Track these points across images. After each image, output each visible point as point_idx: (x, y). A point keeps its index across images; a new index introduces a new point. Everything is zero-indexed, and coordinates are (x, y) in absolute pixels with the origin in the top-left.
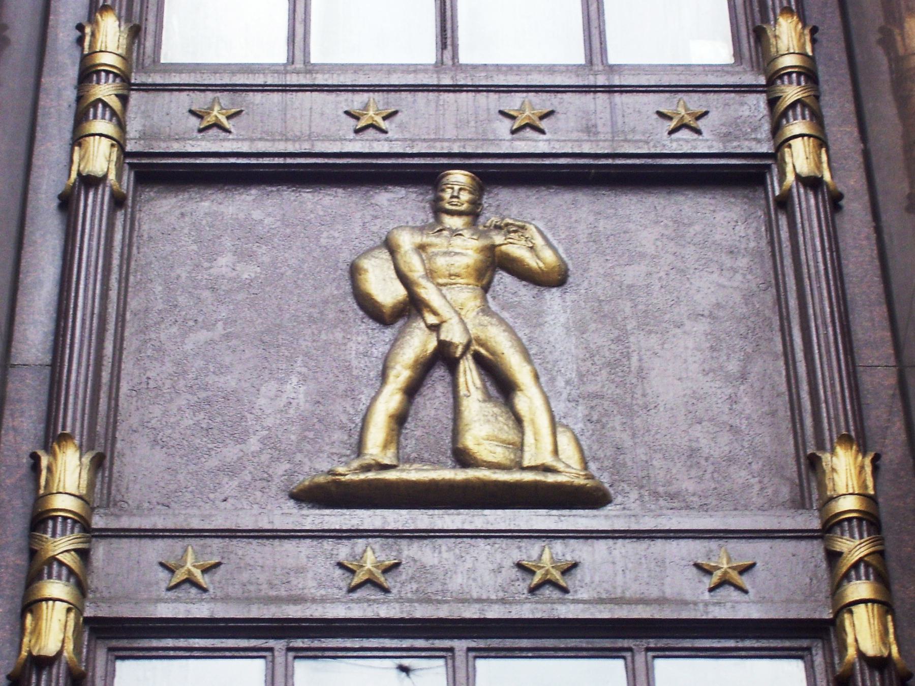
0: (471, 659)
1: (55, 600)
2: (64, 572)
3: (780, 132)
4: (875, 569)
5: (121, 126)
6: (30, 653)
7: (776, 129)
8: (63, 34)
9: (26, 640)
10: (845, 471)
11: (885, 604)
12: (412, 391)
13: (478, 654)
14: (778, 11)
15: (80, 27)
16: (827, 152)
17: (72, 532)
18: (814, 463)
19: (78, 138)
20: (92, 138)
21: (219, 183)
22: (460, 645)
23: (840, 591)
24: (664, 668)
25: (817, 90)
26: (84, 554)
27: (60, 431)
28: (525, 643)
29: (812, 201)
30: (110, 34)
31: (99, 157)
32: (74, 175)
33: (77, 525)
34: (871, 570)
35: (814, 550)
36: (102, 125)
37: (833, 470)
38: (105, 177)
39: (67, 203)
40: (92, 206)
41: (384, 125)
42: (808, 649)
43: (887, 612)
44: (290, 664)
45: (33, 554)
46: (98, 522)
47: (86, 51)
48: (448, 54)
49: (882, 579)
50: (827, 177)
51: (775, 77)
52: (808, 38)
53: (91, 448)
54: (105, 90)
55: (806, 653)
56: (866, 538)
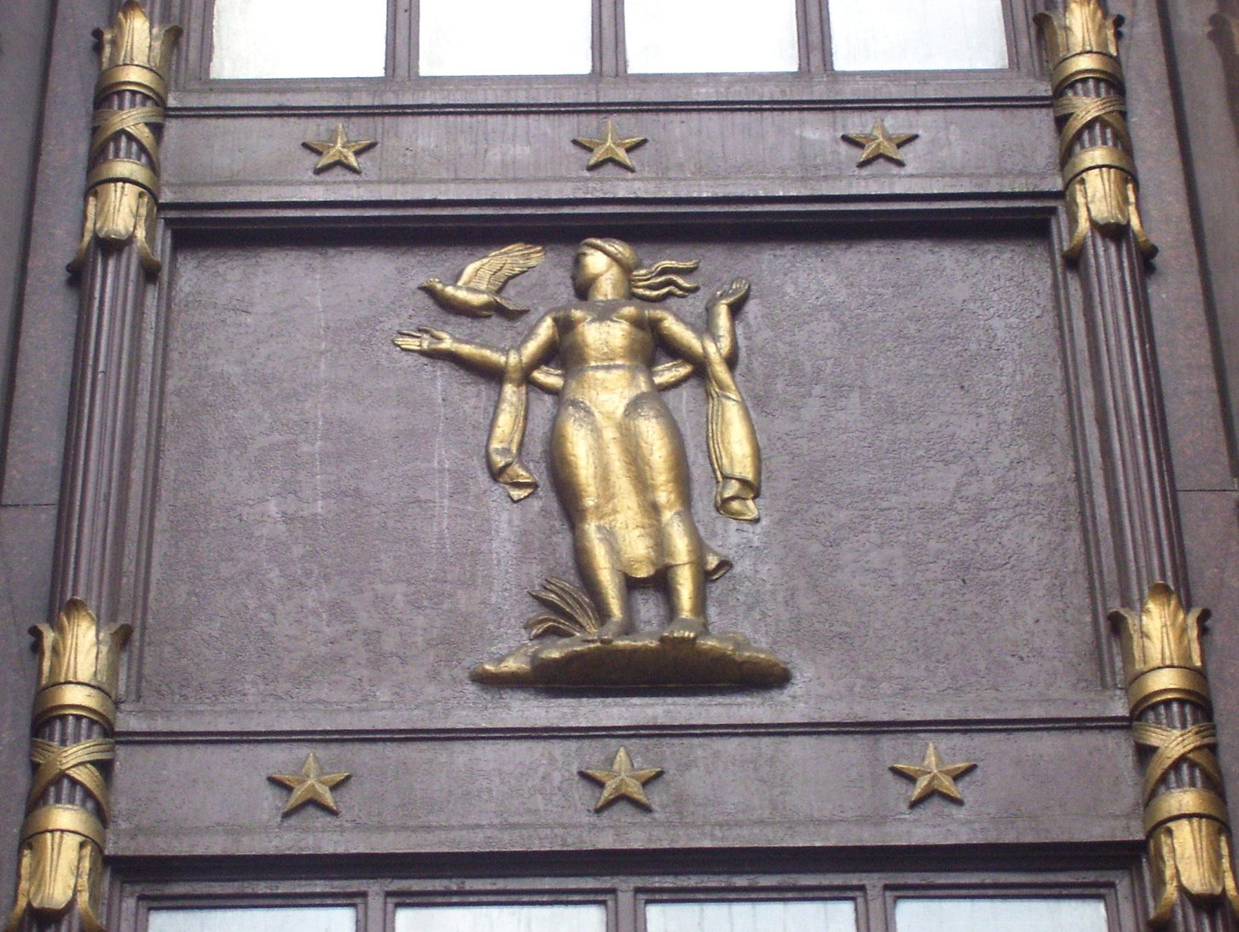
0: (142, 911)
3: (1071, 162)
4: (1203, 771)
6: (29, 904)
9: (24, 885)
11: (1218, 822)
13: (898, 893)
16: (1136, 190)
18: (1117, 625)
19: (95, 186)
21: (459, 244)
22: (374, 888)
25: (1124, 103)
26: (104, 767)
27: (69, 596)
28: (320, 886)
30: (139, 33)
31: (122, 211)
32: (88, 237)
33: (96, 729)
34: (1197, 773)
35: (1118, 747)
38: (131, 239)
40: (112, 281)
42: (364, 895)
43: (1220, 832)
45: (35, 767)
46: (129, 722)
48: (816, 58)
49: (1214, 785)
50: (1135, 222)
51: (1065, 86)
52: (1110, 33)
55: (858, 893)
56: (1190, 727)
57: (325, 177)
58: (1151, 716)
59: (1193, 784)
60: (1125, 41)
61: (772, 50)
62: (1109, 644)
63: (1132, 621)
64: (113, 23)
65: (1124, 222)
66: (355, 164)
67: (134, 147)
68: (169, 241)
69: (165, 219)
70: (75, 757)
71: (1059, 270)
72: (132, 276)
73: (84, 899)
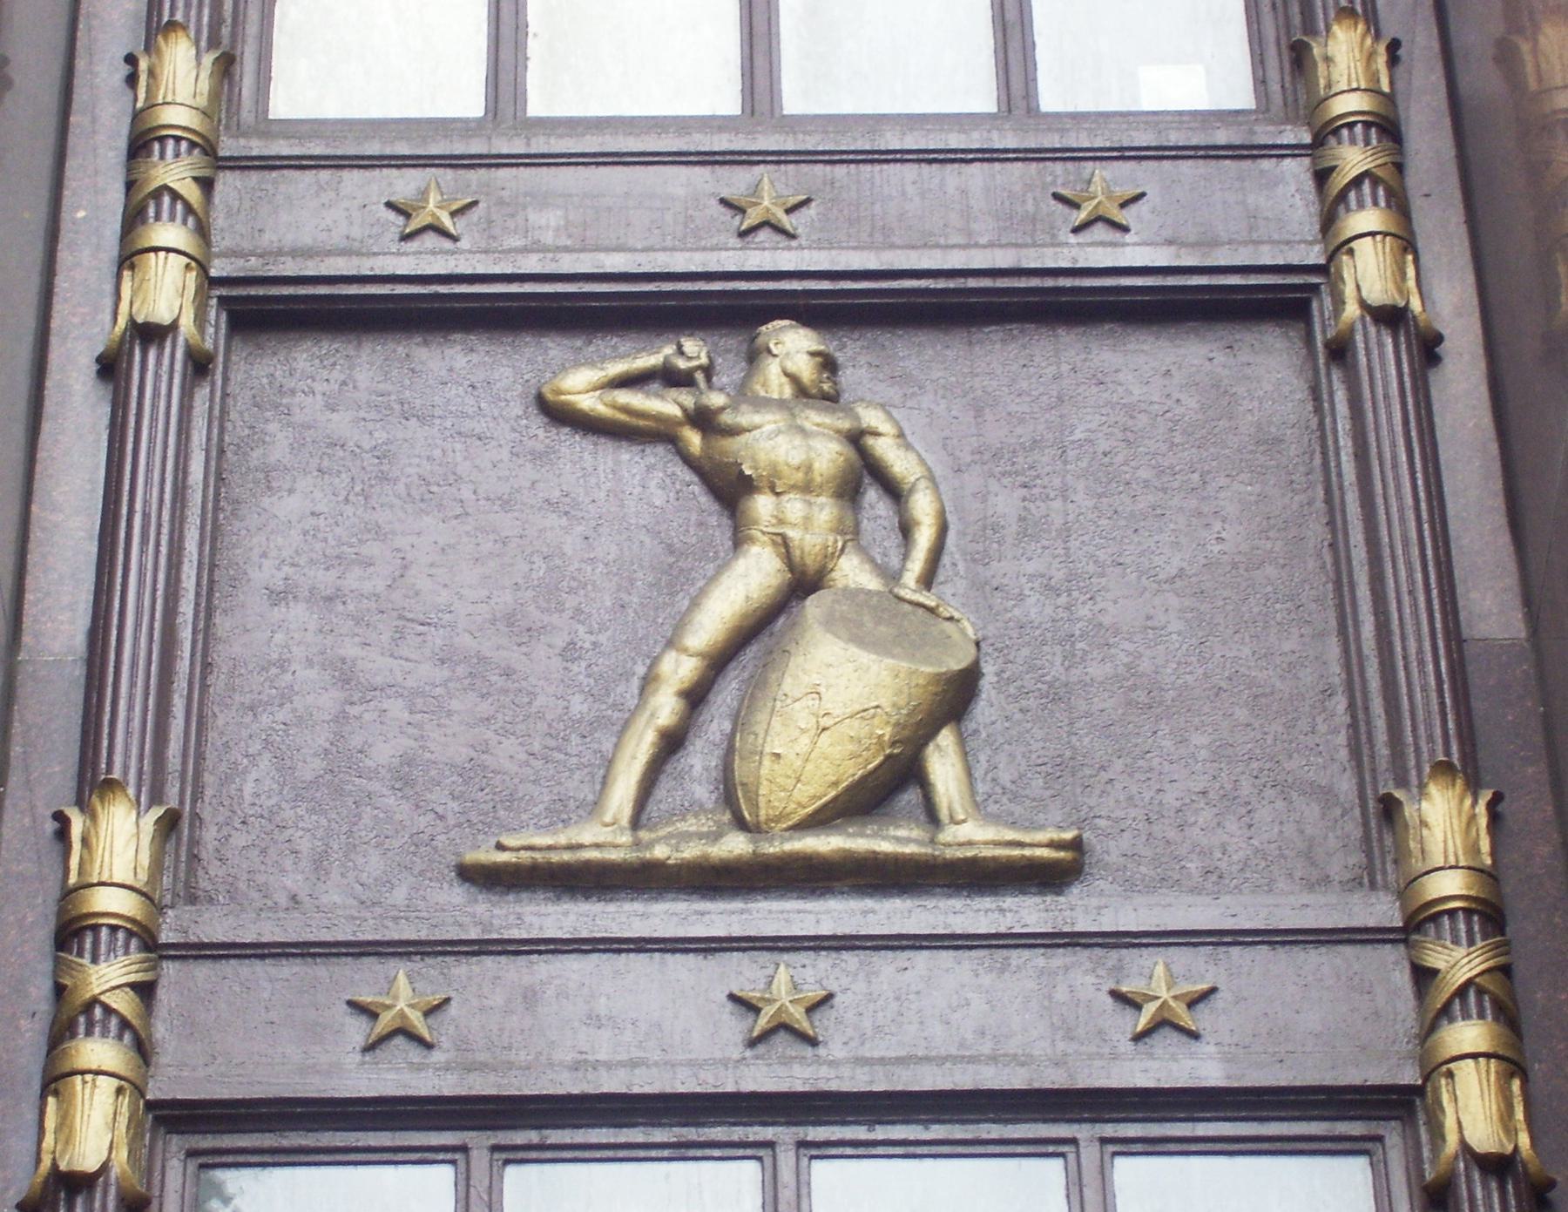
1: (98, 1073)
2: (114, 1022)
5: (202, 231)
6: (55, 1165)
7: (1328, 221)
8: (101, 76)
10: (1443, 820)
11: (1511, 1063)
12: (696, 697)
13: (1117, 1148)
14: (1332, 14)
15: (131, 60)
16: (1416, 261)
17: (127, 953)
18: (1389, 809)
19: (129, 257)
20: (152, 255)
23: (1435, 1037)
24: (1130, 1172)
26: (145, 991)
27: (166, 19)
29: (1390, 348)
30: (183, 75)
32: (122, 322)
34: (1381, 192)
35: (1390, 966)
36: (169, 233)
37: (1424, 824)
39: (110, 367)
40: (157, 374)
41: (787, 222)
43: (1405, 250)
44: (803, 1170)
47: (140, 105)
49: (1507, 1015)
50: (1416, 304)
51: (1326, 133)
53: (156, 798)
54: (174, 171)
56: (1480, 944)
57: (413, 245)
58: (1431, 927)
59: (1481, 1016)
60: (1400, 69)
61: (963, 85)
62: (1380, 832)
63: (1409, 811)
64: (150, 46)
65: (1402, 304)
66: (452, 230)
67: (179, 207)
68: (223, 326)
69: (220, 298)
70: (108, 976)
71: (1373, 824)
72: (178, 366)
73: (122, 1155)
